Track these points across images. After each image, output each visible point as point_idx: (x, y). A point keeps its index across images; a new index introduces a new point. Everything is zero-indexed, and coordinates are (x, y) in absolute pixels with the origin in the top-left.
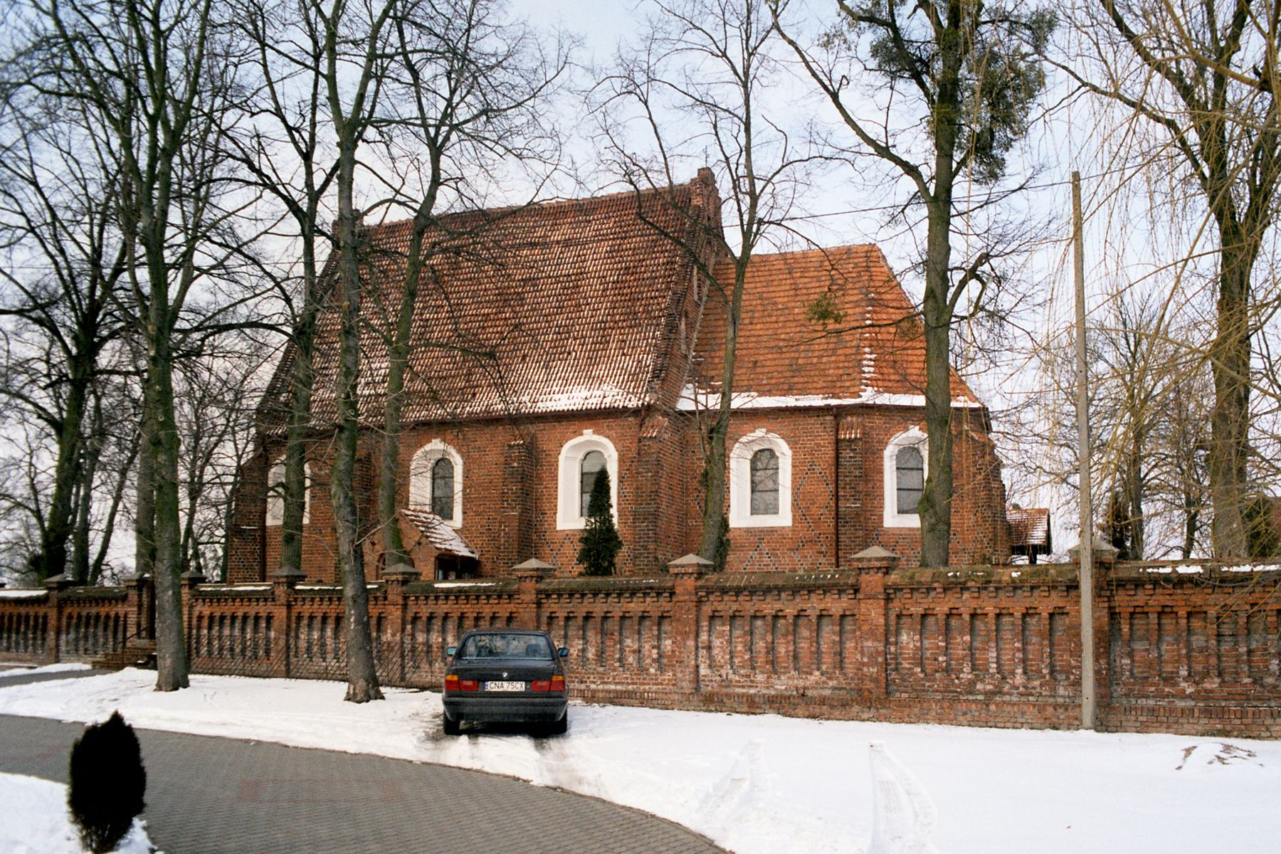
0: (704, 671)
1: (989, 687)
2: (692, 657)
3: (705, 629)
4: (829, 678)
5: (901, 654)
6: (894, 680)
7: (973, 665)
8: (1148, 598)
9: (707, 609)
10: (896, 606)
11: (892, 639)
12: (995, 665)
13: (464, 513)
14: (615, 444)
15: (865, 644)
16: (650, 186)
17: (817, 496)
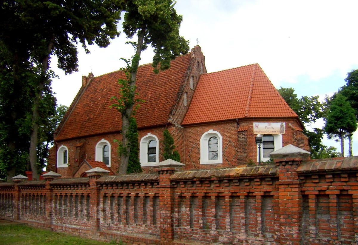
0: (101, 221)
1: (226, 240)
2: (96, 215)
3: (102, 202)
4: (149, 229)
5: (182, 218)
6: (177, 232)
7: (217, 226)
8: (329, 184)
9: (102, 193)
10: (178, 192)
11: (176, 210)
12: (229, 227)
13: (111, 162)
14: (158, 137)
15: (162, 212)
16: (340, 151)
17: (231, 152)
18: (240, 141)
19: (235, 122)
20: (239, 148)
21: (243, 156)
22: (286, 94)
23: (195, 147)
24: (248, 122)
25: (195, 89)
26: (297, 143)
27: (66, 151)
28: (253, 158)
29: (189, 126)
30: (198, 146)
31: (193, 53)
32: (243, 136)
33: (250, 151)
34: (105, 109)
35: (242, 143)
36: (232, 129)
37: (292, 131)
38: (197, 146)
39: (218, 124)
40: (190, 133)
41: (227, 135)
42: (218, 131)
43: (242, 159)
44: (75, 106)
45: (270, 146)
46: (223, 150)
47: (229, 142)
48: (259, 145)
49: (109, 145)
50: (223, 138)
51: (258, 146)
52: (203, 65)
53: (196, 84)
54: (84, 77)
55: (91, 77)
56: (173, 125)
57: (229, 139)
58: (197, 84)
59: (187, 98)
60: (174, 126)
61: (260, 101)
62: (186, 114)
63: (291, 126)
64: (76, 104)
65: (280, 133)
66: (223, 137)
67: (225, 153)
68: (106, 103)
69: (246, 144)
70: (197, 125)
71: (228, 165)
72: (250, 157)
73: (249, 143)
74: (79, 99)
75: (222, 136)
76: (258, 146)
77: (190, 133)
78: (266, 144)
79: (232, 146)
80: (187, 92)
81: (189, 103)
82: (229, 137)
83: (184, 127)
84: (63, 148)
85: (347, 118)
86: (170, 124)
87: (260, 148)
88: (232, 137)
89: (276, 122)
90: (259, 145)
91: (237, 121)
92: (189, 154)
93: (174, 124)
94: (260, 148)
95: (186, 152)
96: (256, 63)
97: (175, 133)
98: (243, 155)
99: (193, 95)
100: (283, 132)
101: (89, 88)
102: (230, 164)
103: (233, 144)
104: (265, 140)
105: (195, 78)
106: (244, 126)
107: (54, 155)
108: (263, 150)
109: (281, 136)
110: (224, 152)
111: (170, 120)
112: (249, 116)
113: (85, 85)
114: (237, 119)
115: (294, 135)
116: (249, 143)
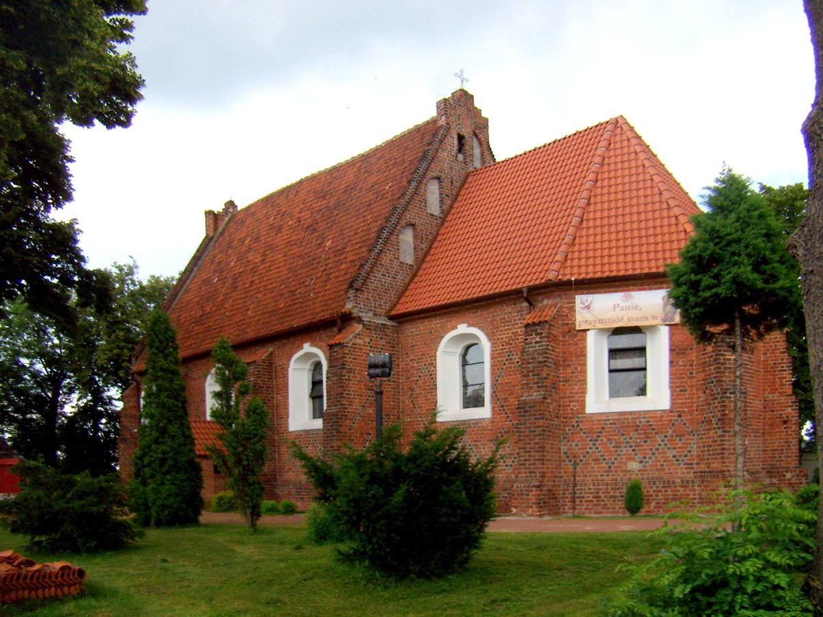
18: (528, 355)
19: (519, 298)
20: (525, 373)
21: (534, 398)
22: (775, 202)
23: (426, 375)
24: (560, 295)
25: (446, 213)
26: (713, 351)
27: (318, 365)
28: (573, 401)
29: (433, 313)
30: (433, 371)
31: (443, 112)
32: (538, 339)
33: (563, 381)
34: (236, 287)
35: (533, 359)
36: (515, 317)
39: (478, 307)
40: (412, 336)
41: (502, 338)
42: (480, 328)
43: (530, 407)
44: (185, 286)
45: (635, 362)
46: (492, 381)
47: (509, 356)
49: (486, 345)
50: (494, 345)
53: (452, 200)
54: (209, 214)
55: (231, 210)
56: (354, 318)
57: (509, 348)
58: (454, 201)
60: (360, 320)
62: (409, 285)
64: (188, 282)
65: (661, 322)
66: (493, 344)
67: (497, 388)
68: (241, 272)
69: (545, 361)
70: (423, 315)
71: (506, 421)
72: (563, 398)
73: (562, 357)
74: (196, 269)
75: (490, 340)
77: (412, 336)
78: (620, 358)
79: (515, 367)
81: (421, 254)
82: (507, 344)
83: (399, 323)
84: (308, 356)
85: (736, 258)
86: (347, 319)
88: (515, 343)
89: (651, 289)
91: (525, 295)
93: (359, 317)
95: (403, 389)
96: (617, 115)
97: (359, 341)
98: (535, 394)
99: (439, 230)
100: (673, 319)
101: (221, 239)
102: (511, 421)
104: (619, 346)
105: (447, 183)
106: (548, 306)
107: (135, 407)
109: (664, 332)
110: (495, 385)
111: (349, 306)
113: (212, 234)
114: (525, 290)
116: (562, 357)
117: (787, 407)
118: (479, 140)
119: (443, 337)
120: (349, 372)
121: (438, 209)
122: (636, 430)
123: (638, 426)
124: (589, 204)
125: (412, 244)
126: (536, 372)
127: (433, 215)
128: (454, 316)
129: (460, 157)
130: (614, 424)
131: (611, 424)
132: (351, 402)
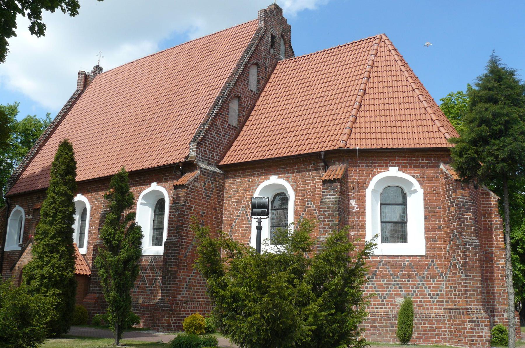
13: (88, 243)
14: (168, 191)
24: (347, 160)
37: (446, 181)
38: (246, 212)
48: (260, 222)
51: (254, 223)
52: (285, 43)
59: (238, 110)
61: (377, 113)
63: (444, 168)
66: (296, 194)
76: (254, 223)
80: (239, 97)
87: (259, 228)
90: (260, 222)
92: (231, 231)
94: (259, 228)
103: (315, 210)
105: (262, 68)
108: (381, 225)
112: (348, 146)
114: (323, 153)
115: (450, 190)
117: (501, 259)
118: (284, 40)
119: (258, 186)
120: (188, 209)
121: (256, 87)
122: (402, 271)
123: (403, 268)
124: (365, 93)
125: (237, 112)
126: (330, 219)
127: (252, 91)
128: (267, 170)
129: (272, 51)
130: (386, 265)
131: (383, 265)
132: (187, 233)
